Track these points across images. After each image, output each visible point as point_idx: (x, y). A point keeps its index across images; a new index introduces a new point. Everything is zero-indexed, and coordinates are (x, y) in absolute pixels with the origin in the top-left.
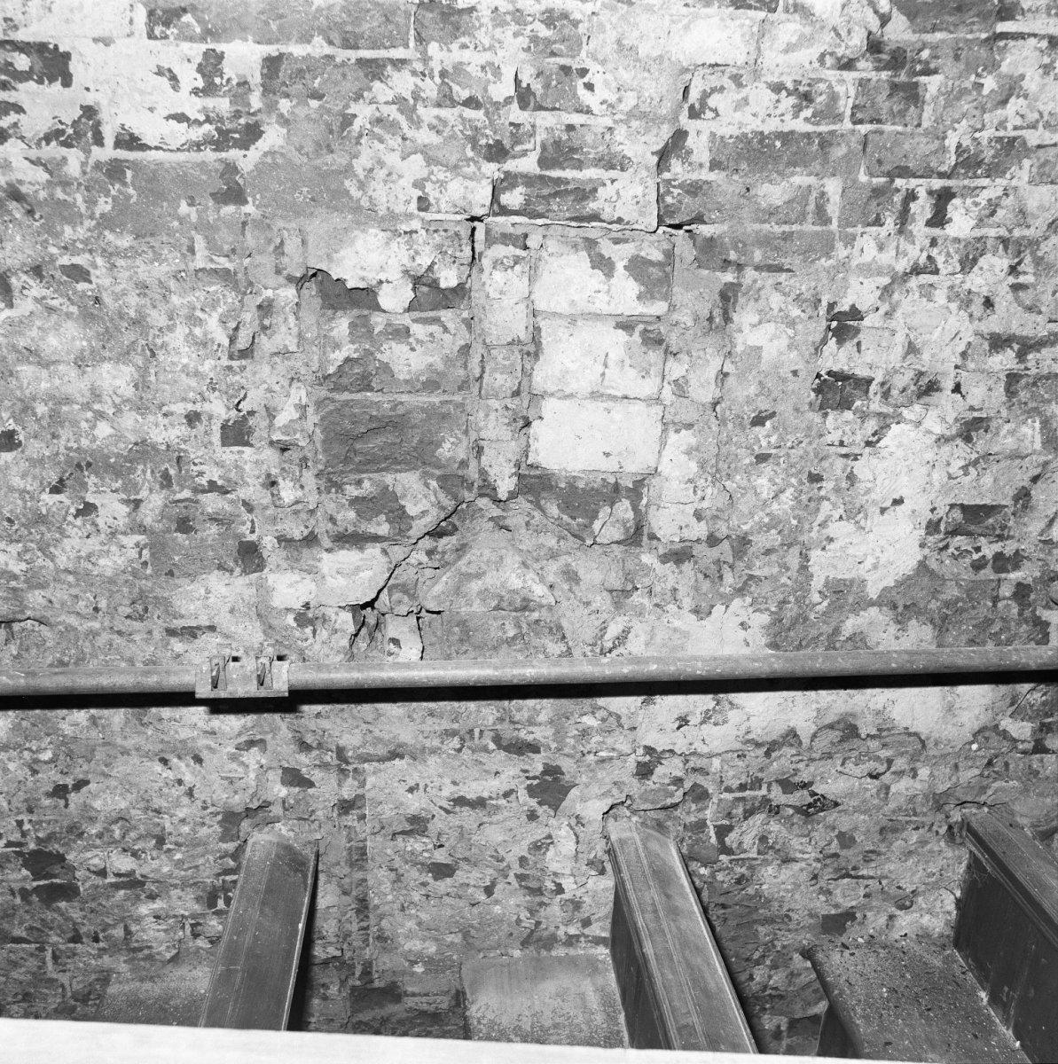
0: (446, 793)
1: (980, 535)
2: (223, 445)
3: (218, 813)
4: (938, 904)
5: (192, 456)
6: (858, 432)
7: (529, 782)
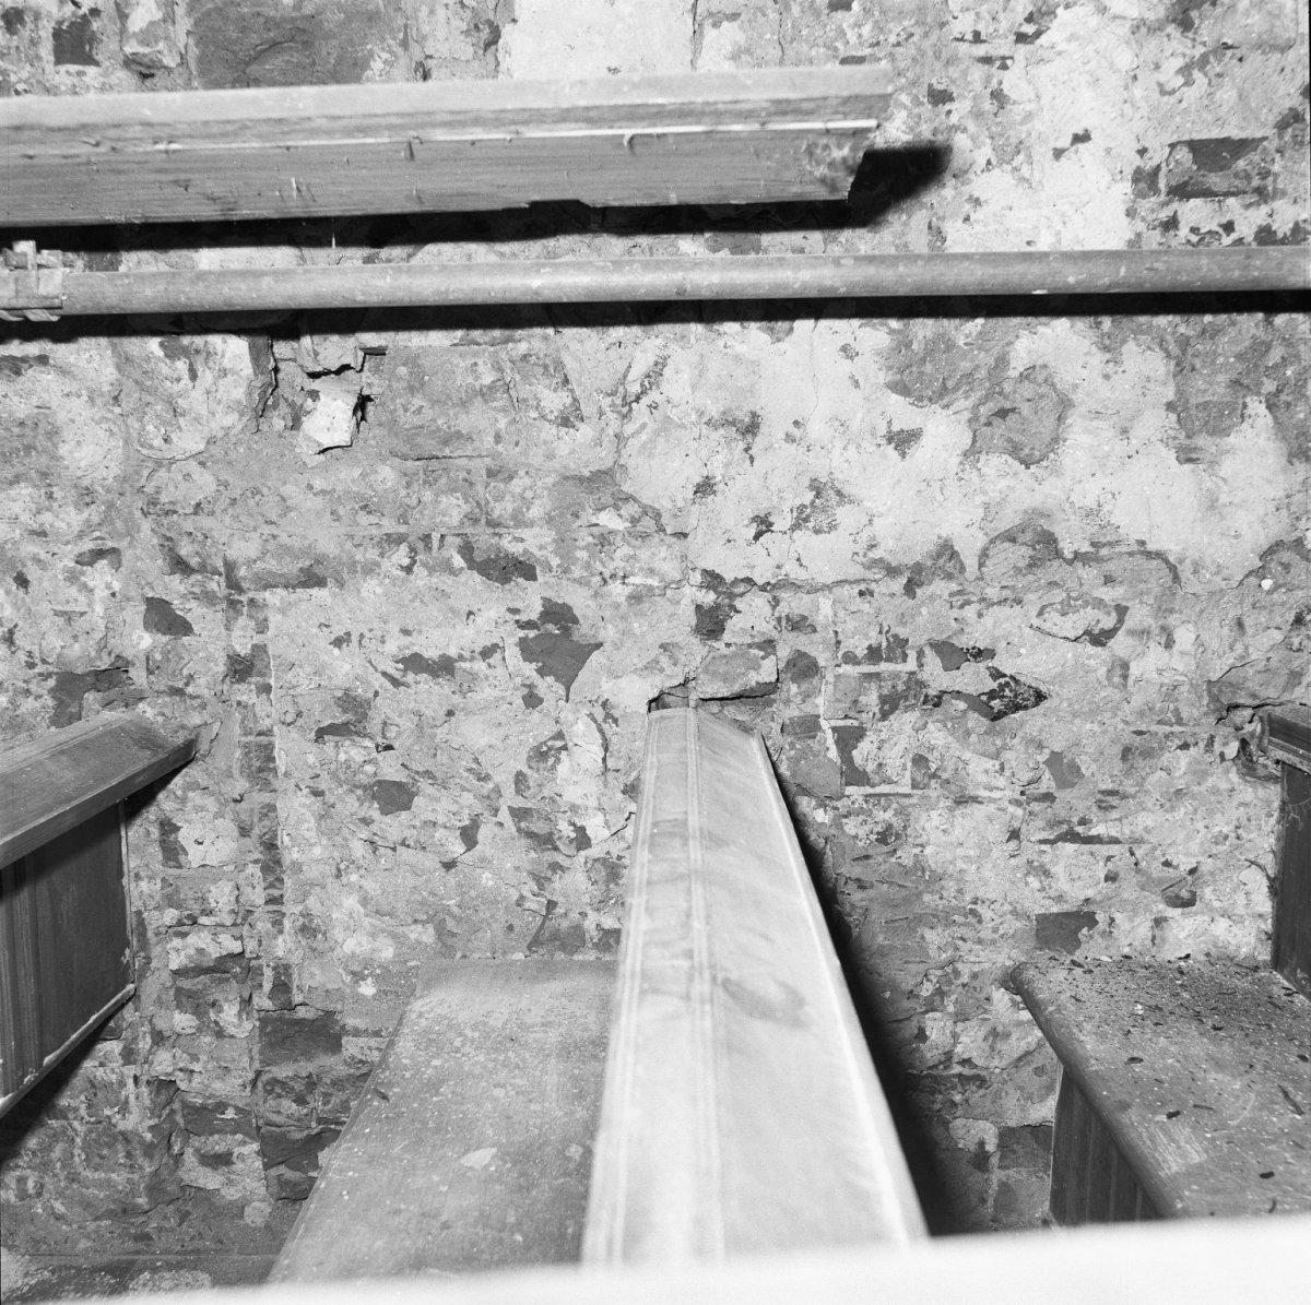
0: (392, 647)
1: (1228, 194)
2: (59, 61)
3: (50, 675)
4: (1240, 898)
5: (13, 78)
6: (1001, 16)
7: (522, 633)
